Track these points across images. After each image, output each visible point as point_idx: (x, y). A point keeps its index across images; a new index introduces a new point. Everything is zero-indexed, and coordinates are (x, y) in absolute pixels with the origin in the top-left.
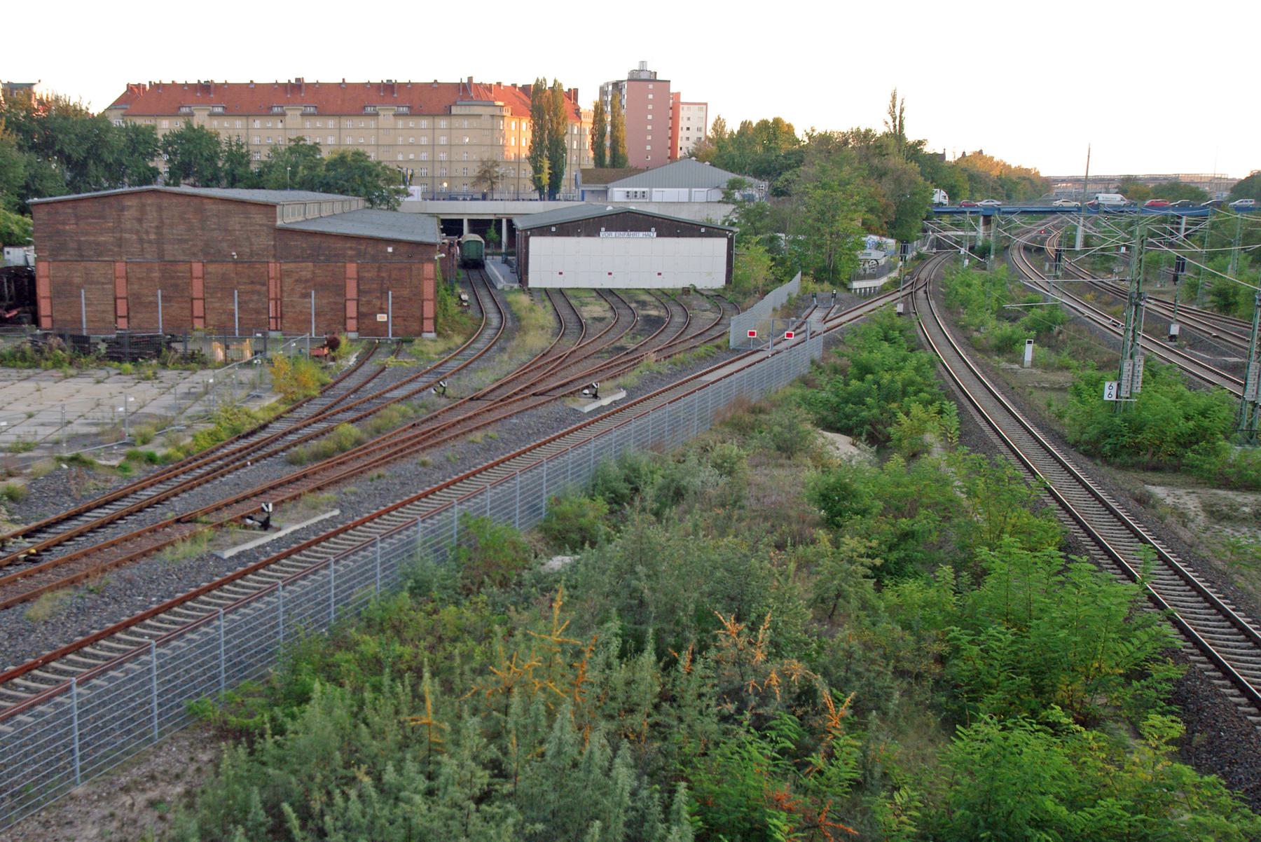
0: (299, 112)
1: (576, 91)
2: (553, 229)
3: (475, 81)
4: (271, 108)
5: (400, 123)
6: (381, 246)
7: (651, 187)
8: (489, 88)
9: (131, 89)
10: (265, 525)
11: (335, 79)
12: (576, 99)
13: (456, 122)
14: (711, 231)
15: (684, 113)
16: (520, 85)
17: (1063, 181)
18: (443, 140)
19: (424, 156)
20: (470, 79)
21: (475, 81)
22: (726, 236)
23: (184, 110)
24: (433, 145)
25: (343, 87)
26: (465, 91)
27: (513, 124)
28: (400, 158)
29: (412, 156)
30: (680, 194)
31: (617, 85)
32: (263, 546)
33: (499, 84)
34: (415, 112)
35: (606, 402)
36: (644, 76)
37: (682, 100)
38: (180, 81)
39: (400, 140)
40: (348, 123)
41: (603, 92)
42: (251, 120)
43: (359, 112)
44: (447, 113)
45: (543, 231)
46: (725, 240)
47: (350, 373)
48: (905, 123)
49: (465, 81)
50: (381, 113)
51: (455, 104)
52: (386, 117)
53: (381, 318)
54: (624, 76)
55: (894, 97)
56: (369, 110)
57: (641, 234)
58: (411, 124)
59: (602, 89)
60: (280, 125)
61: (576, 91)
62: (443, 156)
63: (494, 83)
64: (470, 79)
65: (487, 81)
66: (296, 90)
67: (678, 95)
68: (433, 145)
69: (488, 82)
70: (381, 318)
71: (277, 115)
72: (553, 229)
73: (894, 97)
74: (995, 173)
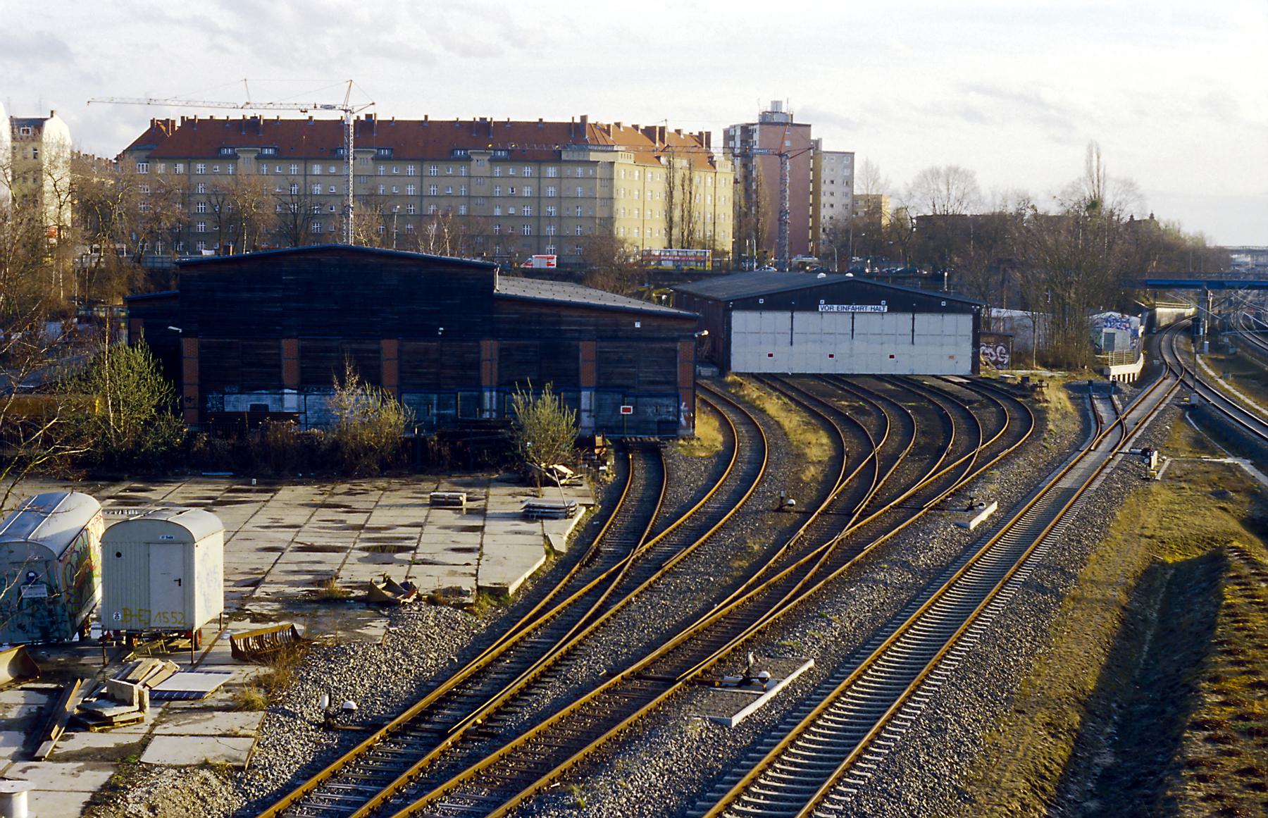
0: (370, 156)
1: (708, 134)
3: (590, 120)
4: (452, 152)
5: (498, 171)
6: (624, 320)
8: (607, 130)
11: (451, 118)
13: (568, 170)
15: (826, 164)
16: (642, 127)
17: (1238, 251)
18: (551, 191)
19: (527, 211)
20: (584, 118)
21: (590, 120)
24: (538, 198)
26: (575, 136)
27: (637, 173)
28: (498, 212)
29: (512, 211)
31: (746, 130)
33: (618, 125)
34: (516, 158)
36: (776, 119)
37: (825, 147)
44: (556, 158)
45: (748, 304)
47: (984, 533)
49: (578, 120)
50: (475, 157)
52: (247, 161)
54: (754, 118)
58: (333, 170)
63: (671, 129)
64: (584, 118)
65: (605, 120)
67: (817, 142)
68: (538, 198)
69: (605, 122)
71: (459, 159)
72: (761, 301)
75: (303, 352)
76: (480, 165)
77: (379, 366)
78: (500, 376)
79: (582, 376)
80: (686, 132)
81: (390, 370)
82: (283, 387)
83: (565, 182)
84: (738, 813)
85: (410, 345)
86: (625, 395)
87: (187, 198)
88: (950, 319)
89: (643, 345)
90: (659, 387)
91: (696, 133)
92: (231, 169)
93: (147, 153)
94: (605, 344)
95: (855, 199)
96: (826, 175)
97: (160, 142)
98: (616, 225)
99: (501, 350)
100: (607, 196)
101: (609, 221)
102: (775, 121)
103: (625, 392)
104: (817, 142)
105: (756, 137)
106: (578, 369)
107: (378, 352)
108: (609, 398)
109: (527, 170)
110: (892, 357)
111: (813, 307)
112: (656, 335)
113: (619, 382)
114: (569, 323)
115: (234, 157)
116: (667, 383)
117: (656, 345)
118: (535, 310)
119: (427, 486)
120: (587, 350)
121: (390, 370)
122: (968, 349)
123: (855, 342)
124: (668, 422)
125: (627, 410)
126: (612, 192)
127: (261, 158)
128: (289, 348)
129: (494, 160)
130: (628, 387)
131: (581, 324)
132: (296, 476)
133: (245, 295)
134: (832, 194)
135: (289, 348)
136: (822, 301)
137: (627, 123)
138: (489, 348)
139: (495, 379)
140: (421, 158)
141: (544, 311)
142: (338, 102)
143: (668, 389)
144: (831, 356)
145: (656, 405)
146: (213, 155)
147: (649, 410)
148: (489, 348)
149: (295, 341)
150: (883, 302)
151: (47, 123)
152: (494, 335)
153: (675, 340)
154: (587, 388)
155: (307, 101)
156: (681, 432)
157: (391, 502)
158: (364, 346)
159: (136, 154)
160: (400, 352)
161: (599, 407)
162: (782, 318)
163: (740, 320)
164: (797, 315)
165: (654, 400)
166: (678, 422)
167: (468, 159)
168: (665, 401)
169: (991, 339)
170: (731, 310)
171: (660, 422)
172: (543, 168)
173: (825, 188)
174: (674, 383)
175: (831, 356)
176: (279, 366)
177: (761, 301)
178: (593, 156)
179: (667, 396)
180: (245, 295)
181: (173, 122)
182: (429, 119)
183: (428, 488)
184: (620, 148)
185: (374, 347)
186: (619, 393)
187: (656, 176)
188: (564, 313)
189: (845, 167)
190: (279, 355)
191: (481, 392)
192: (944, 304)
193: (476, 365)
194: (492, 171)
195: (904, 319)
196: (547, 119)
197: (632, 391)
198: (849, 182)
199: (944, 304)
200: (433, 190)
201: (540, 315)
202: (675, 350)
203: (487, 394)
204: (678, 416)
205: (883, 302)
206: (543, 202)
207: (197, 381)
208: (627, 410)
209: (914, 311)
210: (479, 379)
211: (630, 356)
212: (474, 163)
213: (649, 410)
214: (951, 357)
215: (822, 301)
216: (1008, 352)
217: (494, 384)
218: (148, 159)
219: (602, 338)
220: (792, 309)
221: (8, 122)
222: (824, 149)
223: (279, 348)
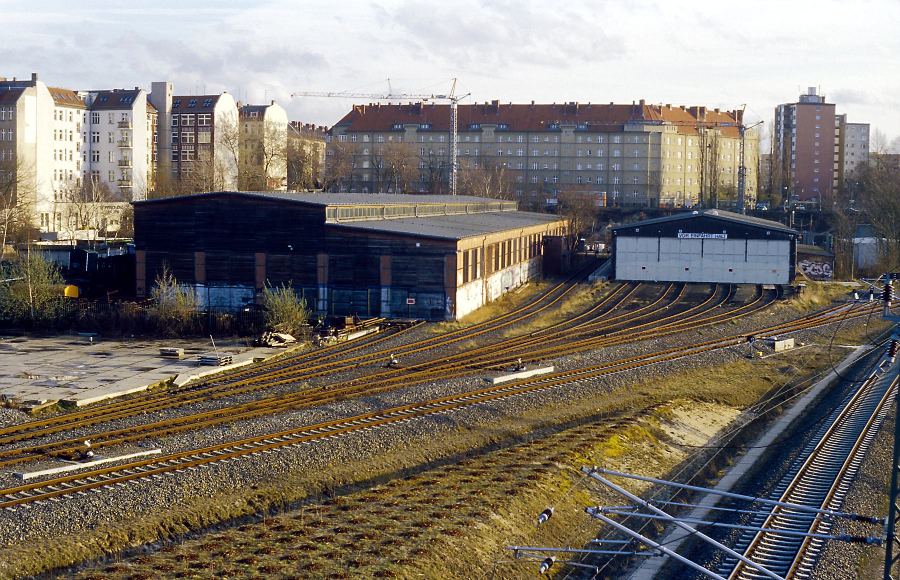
3: (647, 103)
5: (580, 138)
6: (409, 241)
8: (658, 110)
9: (355, 110)
11: (607, 102)
12: (740, 118)
13: (628, 139)
16: (688, 107)
18: (617, 153)
19: (600, 166)
20: (642, 102)
21: (647, 103)
22: (789, 239)
24: (608, 158)
25: (532, 109)
27: (680, 140)
28: (579, 167)
29: (589, 167)
31: (788, 108)
33: (668, 106)
34: (592, 130)
36: (811, 100)
37: (848, 121)
39: (580, 153)
41: (778, 113)
42: (375, 136)
43: (546, 129)
44: (620, 130)
45: (628, 232)
46: (789, 242)
49: (637, 103)
50: (564, 130)
58: (468, 139)
59: (776, 110)
62: (616, 167)
63: (664, 105)
64: (642, 102)
65: (656, 103)
66: (570, 113)
68: (608, 158)
72: (637, 230)
74: (552, 279)
75: (208, 261)
76: (568, 135)
77: (254, 270)
78: (329, 277)
79: (382, 279)
81: (200, 271)
82: (195, 282)
83: (626, 146)
84: (799, 577)
85: (274, 257)
86: (409, 292)
87: (357, 157)
88: (773, 244)
89: (421, 258)
90: (432, 287)
91: (731, 111)
93: (346, 128)
94: (395, 257)
95: (869, 156)
96: (848, 140)
97: (368, 120)
98: (663, 176)
99: (330, 260)
100: (656, 156)
101: (657, 174)
102: (812, 104)
103: (410, 289)
105: (794, 113)
106: (379, 273)
107: (253, 260)
108: (399, 293)
109: (600, 138)
110: (731, 270)
111: (674, 235)
112: (430, 251)
113: (405, 282)
114: (374, 243)
115: (480, 131)
116: (437, 284)
117: (430, 259)
118: (352, 234)
119: (157, 343)
120: (385, 262)
121: (200, 271)
122: (786, 266)
123: (705, 260)
124: (438, 310)
125: (411, 301)
126: (659, 153)
128: (199, 257)
129: (577, 132)
130: (412, 286)
131: (382, 244)
132: (130, 337)
133: (173, 224)
134: (853, 154)
135: (199, 257)
136: (680, 231)
137: (676, 105)
138: (323, 259)
139: (327, 279)
140: (527, 131)
141: (358, 235)
142: (447, 93)
143: (438, 288)
144: (687, 269)
145: (430, 298)
146: (389, 130)
147: (425, 302)
148: (323, 259)
149: (203, 253)
150: (724, 232)
151: (268, 109)
152: (326, 250)
153: (442, 255)
154: (386, 286)
155: (427, 93)
156: (447, 317)
157: (150, 353)
158: (245, 257)
159: (340, 129)
160: (267, 261)
161: (393, 298)
162: (652, 242)
164: (750, 242)
165: (429, 295)
166: (445, 310)
168: (436, 296)
169: (819, 259)
170: (616, 236)
171: (432, 310)
172: (611, 137)
174: (443, 283)
175: (687, 269)
176: (193, 269)
177: (637, 230)
178: (646, 129)
179: (437, 292)
180: (173, 224)
182: (536, 103)
183: (155, 348)
184: (667, 123)
185: (250, 257)
186: (405, 290)
187: (693, 142)
188: (371, 236)
189: (863, 134)
190: (193, 262)
191: (317, 288)
192: (768, 233)
193: (314, 270)
194: (576, 138)
195: (739, 244)
196: (515, 102)
197: (414, 289)
198: (866, 146)
199: (768, 233)
200: (535, 153)
201: (355, 237)
202: (443, 262)
203: (321, 289)
204: (445, 307)
205: (724, 232)
206: (611, 160)
207: (144, 278)
208: (411, 301)
209: (747, 238)
210: (316, 279)
211: (413, 266)
212: (563, 134)
213: (425, 302)
214: (774, 271)
215: (680, 231)
216: (831, 268)
217: (326, 282)
218: (346, 132)
219: (395, 253)
220: (659, 236)
222: (848, 121)
223: (193, 257)
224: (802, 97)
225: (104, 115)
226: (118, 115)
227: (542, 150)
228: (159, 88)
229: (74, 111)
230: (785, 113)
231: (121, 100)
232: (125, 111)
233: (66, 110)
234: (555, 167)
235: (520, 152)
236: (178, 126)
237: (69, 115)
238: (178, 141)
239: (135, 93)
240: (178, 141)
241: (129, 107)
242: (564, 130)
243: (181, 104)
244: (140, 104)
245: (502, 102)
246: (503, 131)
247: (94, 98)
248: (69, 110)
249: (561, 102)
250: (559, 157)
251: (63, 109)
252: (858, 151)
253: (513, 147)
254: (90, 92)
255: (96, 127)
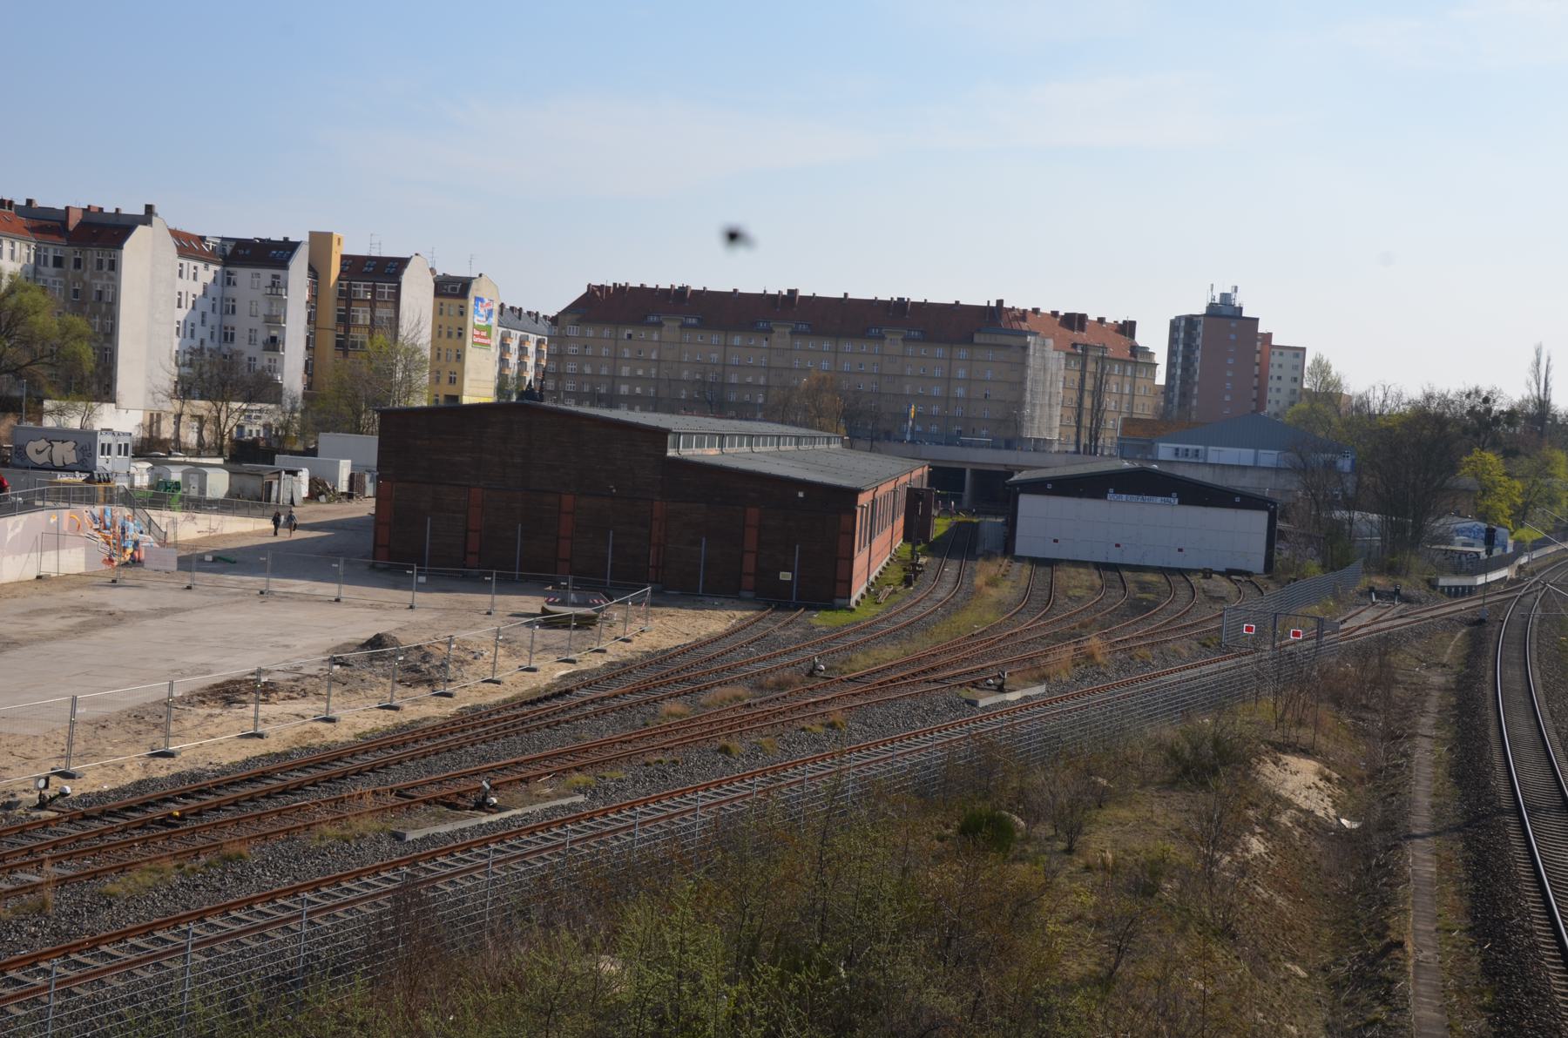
0: (788, 330)
1: (1133, 324)
2: (1049, 486)
5: (910, 350)
7: (1207, 444)
8: (1023, 315)
9: (592, 290)
10: (482, 806)
14: (1249, 502)
15: (1275, 359)
16: (1062, 313)
18: (961, 373)
19: (937, 391)
20: (1000, 302)
22: (1267, 509)
23: (653, 319)
24: (616, 358)
25: (734, 298)
26: (993, 319)
30: (1244, 456)
31: (1191, 321)
32: (464, 830)
33: (1036, 311)
35: (1012, 697)
36: (1226, 311)
37: (1274, 342)
38: (651, 285)
39: (909, 371)
40: (847, 346)
43: (863, 334)
44: (968, 340)
45: (1036, 487)
48: (1551, 384)
49: (993, 304)
50: (776, 330)
51: (979, 331)
52: (894, 344)
53: (785, 576)
55: (1538, 353)
56: (653, 319)
57: (1159, 499)
59: (1172, 322)
60: (765, 344)
61: (1133, 324)
62: (960, 392)
63: (1093, 317)
64: (1000, 302)
67: (1269, 335)
70: (785, 576)
72: (1049, 486)
73: (1538, 353)
80: (1109, 320)
92: (656, 337)
97: (607, 307)
104: (1269, 335)
105: (1200, 329)
115: (659, 325)
127: (684, 326)
129: (794, 333)
137: (1046, 309)
159: (569, 317)
163: (1026, 503)
167: (882, 338)
173: (1272, 384)
181: (1128, 328)
192: (1238, 500)
199: (1238, 500)
200: (735, 360)
218: (579, 322)
221: (467, 275)
222: (1274, 342)
224: (1211, 306)
225: (243, 274)
226: (266, 274)
227: (857, 362)
228: (321, 242)
229: (201, 265)
230: (1184, 330)
231: (273, 254)
232: (276, 272)
233: (190, 264)
234: (762, 381)
235: (604, 352)
236: (346, 296)
237: (192, 271)
238: (345, 319)
239: (289, 247)
240: (345, 319)
241: (284, 265)
242: (889, 337)
243: (356, 266)
244: (298, 268)
245: (804, 291)
246: (914, 340)
247: (229, 250)
248: (193, 263)
249: (884, 296)
250: (658, 361)
251: (185, 262)
252: (1286, 385)
253: (816, 359)
254: (223, 239)
255: (231, 292)
